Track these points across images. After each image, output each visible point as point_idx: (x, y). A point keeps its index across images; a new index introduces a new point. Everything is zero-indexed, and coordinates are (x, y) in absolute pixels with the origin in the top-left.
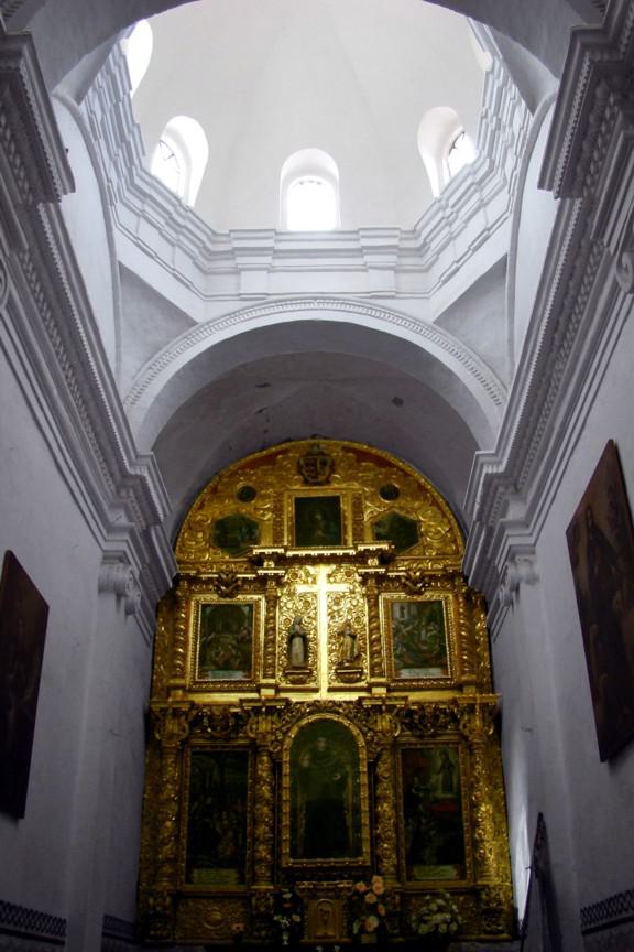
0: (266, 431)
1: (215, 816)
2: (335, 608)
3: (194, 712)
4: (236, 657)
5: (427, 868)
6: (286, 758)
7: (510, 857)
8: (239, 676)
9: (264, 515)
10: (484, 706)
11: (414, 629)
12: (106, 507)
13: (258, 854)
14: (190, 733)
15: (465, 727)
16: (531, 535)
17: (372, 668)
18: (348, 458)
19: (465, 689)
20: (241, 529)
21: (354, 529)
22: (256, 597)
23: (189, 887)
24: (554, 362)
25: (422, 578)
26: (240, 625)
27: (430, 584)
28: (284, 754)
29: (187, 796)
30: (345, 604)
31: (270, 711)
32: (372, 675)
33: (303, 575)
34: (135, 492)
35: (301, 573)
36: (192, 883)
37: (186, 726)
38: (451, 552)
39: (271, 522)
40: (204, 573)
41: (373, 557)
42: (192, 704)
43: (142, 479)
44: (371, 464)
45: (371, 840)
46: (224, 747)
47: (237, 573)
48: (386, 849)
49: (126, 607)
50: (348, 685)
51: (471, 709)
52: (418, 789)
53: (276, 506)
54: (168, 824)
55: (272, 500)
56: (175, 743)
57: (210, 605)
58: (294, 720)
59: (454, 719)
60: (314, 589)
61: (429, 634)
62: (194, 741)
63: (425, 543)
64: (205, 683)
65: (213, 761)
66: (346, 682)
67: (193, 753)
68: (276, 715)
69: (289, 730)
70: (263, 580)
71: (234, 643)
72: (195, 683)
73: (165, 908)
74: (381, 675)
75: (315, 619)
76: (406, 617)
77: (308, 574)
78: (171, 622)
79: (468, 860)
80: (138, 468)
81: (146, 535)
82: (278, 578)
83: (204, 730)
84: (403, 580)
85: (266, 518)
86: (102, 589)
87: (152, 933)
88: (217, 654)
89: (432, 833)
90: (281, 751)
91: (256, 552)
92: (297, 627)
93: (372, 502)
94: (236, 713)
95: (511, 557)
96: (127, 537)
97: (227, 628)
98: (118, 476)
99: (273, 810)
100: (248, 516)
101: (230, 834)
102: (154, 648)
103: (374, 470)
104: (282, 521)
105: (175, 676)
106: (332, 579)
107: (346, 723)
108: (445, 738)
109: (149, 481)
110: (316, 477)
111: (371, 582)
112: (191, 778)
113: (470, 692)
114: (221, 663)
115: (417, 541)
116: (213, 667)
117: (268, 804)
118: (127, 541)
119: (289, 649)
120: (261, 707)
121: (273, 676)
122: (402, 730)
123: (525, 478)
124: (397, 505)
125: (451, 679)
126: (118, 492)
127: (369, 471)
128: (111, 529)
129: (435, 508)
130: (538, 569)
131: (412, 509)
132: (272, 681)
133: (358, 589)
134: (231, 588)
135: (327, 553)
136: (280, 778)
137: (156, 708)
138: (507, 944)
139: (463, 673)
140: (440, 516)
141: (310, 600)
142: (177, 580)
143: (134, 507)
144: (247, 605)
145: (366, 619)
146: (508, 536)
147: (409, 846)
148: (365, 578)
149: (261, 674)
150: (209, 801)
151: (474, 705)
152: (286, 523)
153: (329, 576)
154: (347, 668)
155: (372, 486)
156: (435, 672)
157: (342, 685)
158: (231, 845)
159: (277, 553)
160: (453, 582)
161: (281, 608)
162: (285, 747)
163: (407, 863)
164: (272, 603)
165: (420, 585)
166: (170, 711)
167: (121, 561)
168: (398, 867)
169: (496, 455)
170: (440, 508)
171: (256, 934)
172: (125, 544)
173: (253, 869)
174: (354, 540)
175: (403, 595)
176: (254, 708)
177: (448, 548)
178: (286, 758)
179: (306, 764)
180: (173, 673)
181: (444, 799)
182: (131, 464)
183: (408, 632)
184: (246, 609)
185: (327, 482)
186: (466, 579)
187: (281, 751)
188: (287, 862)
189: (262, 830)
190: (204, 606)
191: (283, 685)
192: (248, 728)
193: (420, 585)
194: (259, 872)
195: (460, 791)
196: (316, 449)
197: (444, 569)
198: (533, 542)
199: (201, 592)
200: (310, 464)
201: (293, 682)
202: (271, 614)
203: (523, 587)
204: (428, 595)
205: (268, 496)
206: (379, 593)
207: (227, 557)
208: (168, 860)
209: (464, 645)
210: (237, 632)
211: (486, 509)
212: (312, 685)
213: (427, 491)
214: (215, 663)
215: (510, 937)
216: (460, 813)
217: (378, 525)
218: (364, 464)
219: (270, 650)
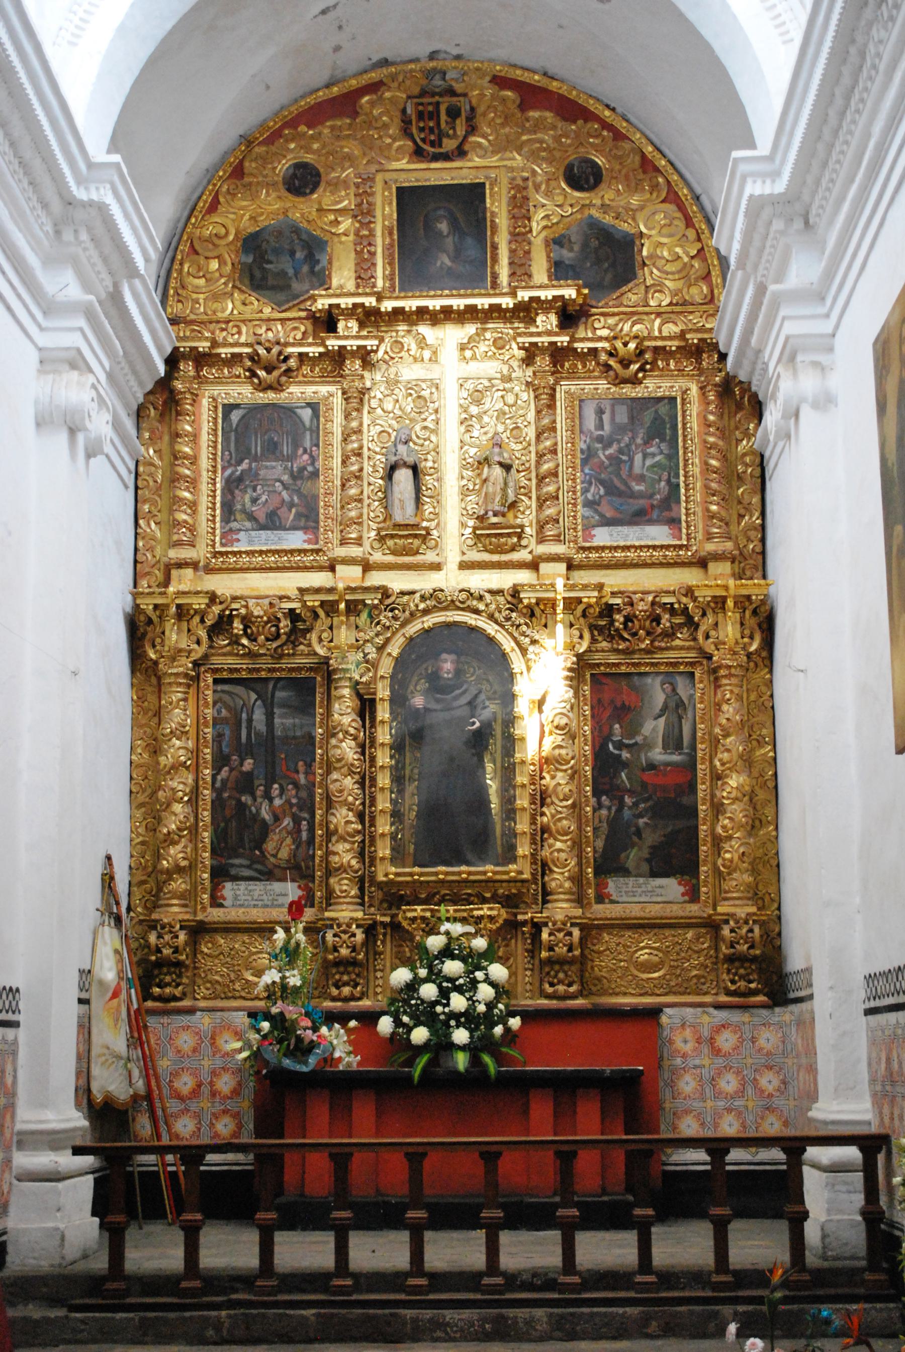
0: (337, 49)
1: (261, 790)
2: (474, 410)
3: (216, 609)
4: (292, 505)
5: (631, 881)
6: (383, 691)
7: (778, 866)
8: (296, 540)
9: (336, 223)
10: (743, 602)
11: (620, 451)
12: (33, 260)
13: (337, 859)
14: (211, 647)
15: (707, 637)
16: (827, 316)
17: (541, 527)
18: (504, 100)
19: (711, 566)
20: (292, 253)
21: (512, 252)
22: (324, 390)
23: (215, 915)
24: (870, 25)
25: (640, 352)
26: (296, 444)
27: (654, 363)
28: (380, 685)
29: (209, 757)
30: (492, 403)
31: (353, 608)
32: (541, 539)
33: (413, 347)
34: (90, 229)
35: (409, 342)
36: (221, 906)
37: (203, 634)
38: (698, 300)
39: (352, 237)
40: (225, 344)
41: (546, 311)
42: (213, 598)
43: (102, 209)
44: (548, 114)
45: (533, 836)
46: (273, 670)
47: (287, 344)
48: (559, 851)
49: (86, 449)
50: (495, 558)
51: (719, 603)
52: (620, 746)
53: (359, 205)
54: (177, 808)
55: (352, 191)
56: (185, 665)
57: (237, 406)
58: (397, 624)
59: (691, 623)
60: (434, 373)
61: (649, 462)
62: (217, 661)
63: (649, 282)
64: (234, 553)
65: (254, 696)
66: (491, 552)
67: (216, 681)
68: (364, 615)
69: (387, 641)
70: (339, 357)
71: (285, 478)
72: (216, 554)
73: (176, 950)
74: (558, 539)
75: (435, 431)
76: (607, 427)
77: (422, 343)
78: (166, 438)
79: (703, 869)
80: (92, 188)
81: (116, 298)
82: (365, 357)
83: (235, 641)
84: (603, 357)
85: (342, 228)
86: (40, 423)
87: (156, 990)
88: (254, 501)
89: (641, 821)
90: (374, 679)
91: (322, 303)
92: (402, 449)
93: (548, 194)
94: (292, 611)
95: (790, 358)
96: (82, 322)
97: (272, 449)
98: (56, 206)
99: (362, 783)
100: (305, 225)
101: (287, 822)
102: (137, 488)
103: (554, 128)
104: (372, 234)
105: (179, 544)
106: (468, 354)
107: (491, 629)
108: (672, 654)
109: (116, 211)
110: (437, 143)
111: (543, 362)
112: (214, 725)
113: (721, 570)
114: (262, 517)
115: (634, 276)
116: (248, 524)
117: (351, 773)
118: (81, 330)
119: (386, 500)
120: (337, 602)
121: (359, 542)
122: (594, 640)
123: (822, 207)
124: (597, 202)
125: (687, 547)
126: (58, 233)
127: (545, 129)
128: (50, 307)
129: (671, 208)
130: (834, 381)
131: (627, 209)
132: (355, 551)
133: (518, 373)
134: (276, 373)
135: (458, 303)
136: (373, 725)
137: (147, 605)
138: (764, 1012)
139: (709, 537)
140: (680, 224)
141: (426, 394)
142: (173, 361)
143: (89, 258)
144: (309, 405)
145: (531, 433)
146: (784, 319)
147: (600, 844)
148: (530, 354)
149: (335, 537)
150: (248, 765)
151: (724, 599)
152: (379, 241)
153: (462, 348)
154: (495, 526)
155: (550, 161)
156: (658, 534)
157: (486, 557)
158: (289, 840)
159: (362, 305)
160: (699, 361)
161: (372, 411)
162: (381, 673)
163: (597, 873)
164: (354, 403)
165: (635, 367)
166: (173, 609)
167: (73, 366)
168: (578, 879)
169: (770, 158)
170: (681, 207)
171: (335, 992)
172: (79, 334)
173: (327, 884)
174: (512, 275)
175: (603, 385)
176: (323, 604)
177: (694, 290)
178: (383, 691)
179: (418, 701)
180: (175, 537)
181: (667, 764)
182: (79, 183)
183: (609, 457)
184: (306, 414)
185: (461, 152)
186: (723, 357)
187: (374, 679)
188: (386, 871)
189: (343, 818)
190: (229, 409)
191: (377, 557)
192: (314, 637)
193: (635, 367)
194: (337, 888)
195: (694, 748)
196: (437, 81)
197: (682, 335)
198: (830, 330)
199: (218, 381)
200: (428, 115)
201: (394, 553)
202: (354, 424)
203: (806, 413)
204: (653, 386)
205: (345, 184)
206: (557, 382)
207: (267, 310)
208: (179, 870)
209: (714, 485)
210: (291, 458)
211: (753, 252)
212: (430, 557)
213: (657, 170)
214: (251, 517)
215: (770, 1002)
216: (692, 788)
217: (558, 242)
218: (534, 114)
219: (353, 492)
